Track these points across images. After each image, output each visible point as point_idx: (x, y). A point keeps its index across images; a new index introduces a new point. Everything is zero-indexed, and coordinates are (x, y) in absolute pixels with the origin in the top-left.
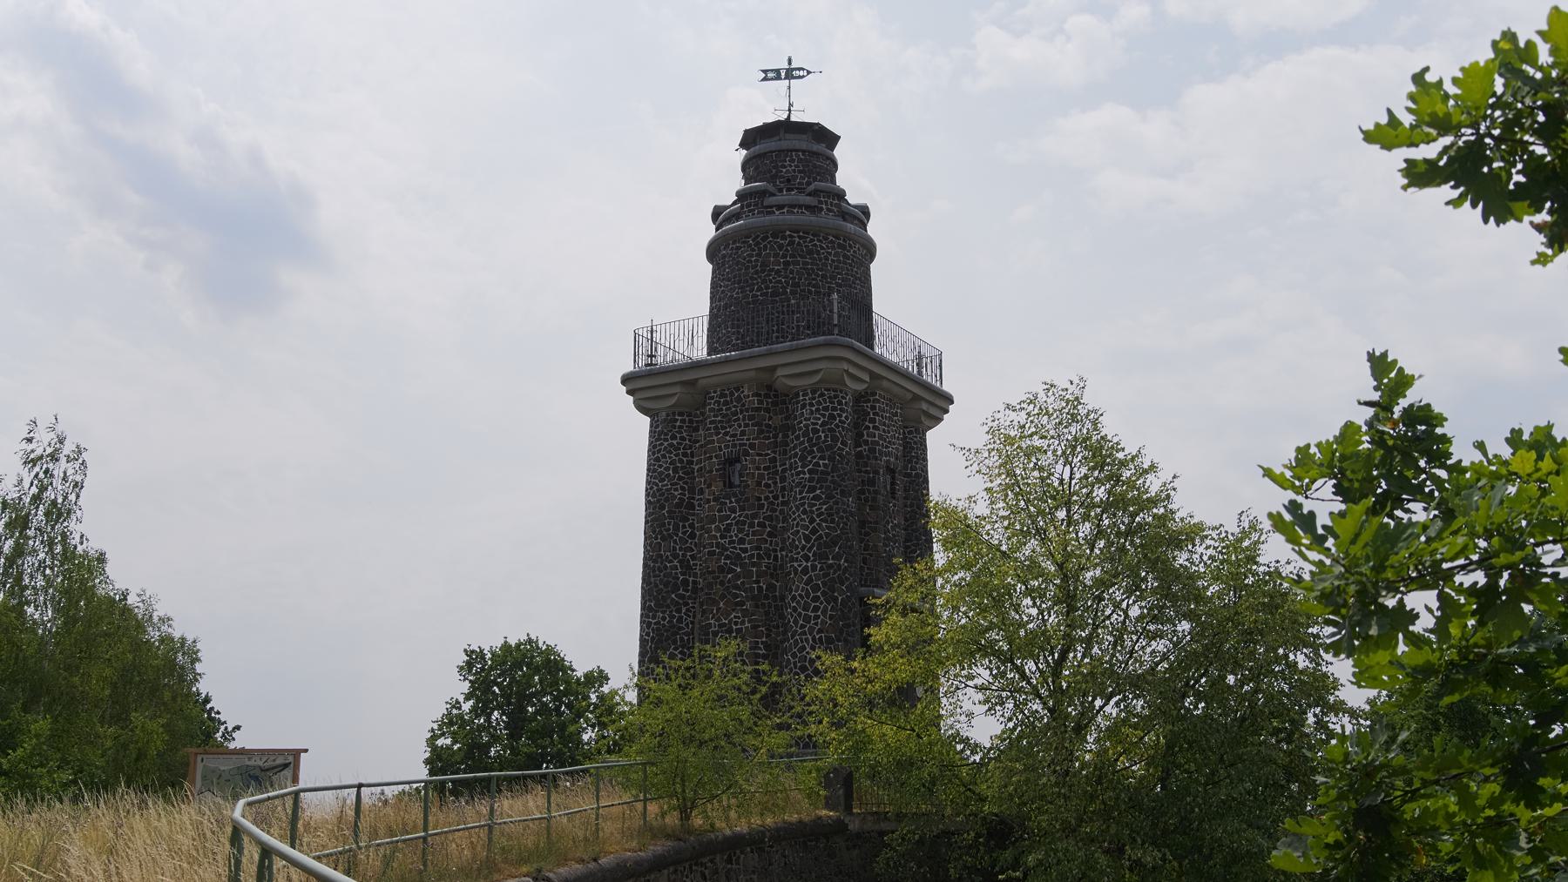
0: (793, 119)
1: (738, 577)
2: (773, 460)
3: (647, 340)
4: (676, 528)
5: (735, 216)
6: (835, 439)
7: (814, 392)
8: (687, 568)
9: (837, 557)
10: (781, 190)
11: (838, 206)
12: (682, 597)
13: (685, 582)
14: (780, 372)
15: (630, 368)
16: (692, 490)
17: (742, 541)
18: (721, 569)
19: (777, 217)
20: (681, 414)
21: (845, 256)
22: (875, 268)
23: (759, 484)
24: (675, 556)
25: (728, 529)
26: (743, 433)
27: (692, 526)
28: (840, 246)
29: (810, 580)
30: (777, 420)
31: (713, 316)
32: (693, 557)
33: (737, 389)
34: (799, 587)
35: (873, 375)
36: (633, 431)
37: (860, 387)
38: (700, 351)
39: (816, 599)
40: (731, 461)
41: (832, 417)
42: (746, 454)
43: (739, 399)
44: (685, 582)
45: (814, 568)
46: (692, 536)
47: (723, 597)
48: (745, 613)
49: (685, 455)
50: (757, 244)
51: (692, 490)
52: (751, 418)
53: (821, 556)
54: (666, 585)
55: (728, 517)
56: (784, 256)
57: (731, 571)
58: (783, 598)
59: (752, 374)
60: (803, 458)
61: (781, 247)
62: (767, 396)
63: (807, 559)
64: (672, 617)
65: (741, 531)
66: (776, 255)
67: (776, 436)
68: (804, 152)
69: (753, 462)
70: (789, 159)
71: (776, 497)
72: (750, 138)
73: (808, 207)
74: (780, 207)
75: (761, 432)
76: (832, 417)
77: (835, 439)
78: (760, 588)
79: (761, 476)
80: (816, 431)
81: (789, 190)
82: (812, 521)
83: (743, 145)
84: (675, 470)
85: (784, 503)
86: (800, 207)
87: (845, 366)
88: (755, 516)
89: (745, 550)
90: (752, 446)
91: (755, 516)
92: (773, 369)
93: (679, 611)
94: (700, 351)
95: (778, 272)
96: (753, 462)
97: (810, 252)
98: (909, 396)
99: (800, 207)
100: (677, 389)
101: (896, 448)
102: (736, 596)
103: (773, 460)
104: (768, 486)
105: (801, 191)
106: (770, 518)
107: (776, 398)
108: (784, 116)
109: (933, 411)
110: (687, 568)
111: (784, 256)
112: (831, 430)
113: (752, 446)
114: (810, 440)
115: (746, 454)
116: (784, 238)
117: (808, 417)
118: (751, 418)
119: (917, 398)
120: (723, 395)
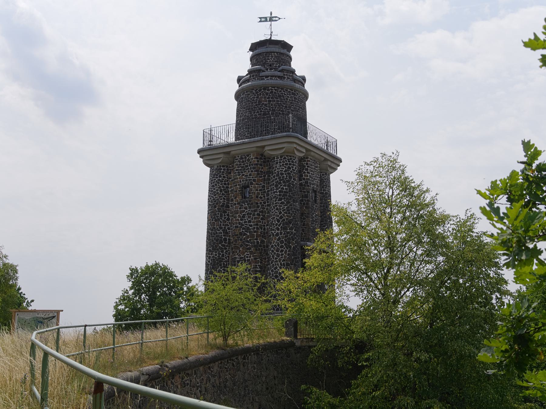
0: (273, 38)
1: (248, 237)
2: (264, 186)
3: (209, 134)
4: (221, 216)
5: (247, 81)
6: (290, 177)
7: (281, 157)
8: (226, 233)
9: (291, 229)
10: (267, 69)
11: (292, 76)
12: (224, 245)
13: (225, 239)
14: (266, 148)
15: (201, 146)
16: (228, 200)
17: (250, 222)
18: (241, 234)
19: (266, 81)
20: (223, 166)
21: (295, 98)
22: (308, 103)
23: (257, 197)
24: (221, 228)
25: (244, 217)
26: (250, 175)
27: (228, 215)
28: (293, 94)
29: (279, 239)
30: (266, 169)
31: (237, 124)
32: (229, 229)
33: (248, 156)
34: (275, 242)
35: (307, 150)
36: (204, 173)
37: (302, 155)
38: (232, 139)
39: (282, 247)
40: (245, 187)
41: (289, 168)
42: (252, 184)
43: (249, 160)
44: (225, 239)
45: (281, 233)
46: (228, 219)
47: (241, 246)
48: (251, 253)
49: (225, 184)
50: (257, 93)
51: (228, 200)
52: (254, 168)
53: (285, 228)
54: (217, 240)
55: (244, 211)
56: (268, 98)
57: (245, 234)
58: (267, 246)
59: (255, 149)
60: (276, 186)
61: (267, 94)
62: (261, 159)
63: (278, 229)
64: (220, 254)
65: (249, 217)
66: (265, 98)
67: (264, 176)
68: (277, 53)
69: (255, 187)
70: (271, 56)
71: (265, 203)
72: (254, 47)
73: (279, 77)
74: (267, 77)
75: (258, 174)
76: (289, 168)
77: (290, 177)
78: (258, 242)
79: (258, 194)
80: (282, 174)
81: (271, 69)
82: (280, 213)
83: (251, 49)
84: (221, 191)
85: (268, 205)
86: (276, 76)
87: (295, 146)
88: (255, 211)
89: (251, 226)
90: (254, 180)
91: (255, 211)
92: (263, 147)
93: (222, 252)
94: (232, 139)
95: (266, 105)
96: (255, 187)
97: (280, 96)
98: (323, 159)
99: (276, 76)
100: (222, 156)
101: (317, 181)
102: (247, 245)
103: (264, 186)
104: (261, 198)
105: (276, 69)
106: (262, 212)
107: (265, 160)
108: (268, 37)
109: (333, 165)
110: (226, 233)
111: (268, 98)
112: (289, 173)
113: (254, 180)
114: (280, 178)
115: (252, 184)
116: (268, 90)
117: (278, 168)
118: (254, 168)
119: (326, 160)
120: (242, 158)
